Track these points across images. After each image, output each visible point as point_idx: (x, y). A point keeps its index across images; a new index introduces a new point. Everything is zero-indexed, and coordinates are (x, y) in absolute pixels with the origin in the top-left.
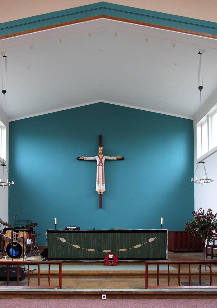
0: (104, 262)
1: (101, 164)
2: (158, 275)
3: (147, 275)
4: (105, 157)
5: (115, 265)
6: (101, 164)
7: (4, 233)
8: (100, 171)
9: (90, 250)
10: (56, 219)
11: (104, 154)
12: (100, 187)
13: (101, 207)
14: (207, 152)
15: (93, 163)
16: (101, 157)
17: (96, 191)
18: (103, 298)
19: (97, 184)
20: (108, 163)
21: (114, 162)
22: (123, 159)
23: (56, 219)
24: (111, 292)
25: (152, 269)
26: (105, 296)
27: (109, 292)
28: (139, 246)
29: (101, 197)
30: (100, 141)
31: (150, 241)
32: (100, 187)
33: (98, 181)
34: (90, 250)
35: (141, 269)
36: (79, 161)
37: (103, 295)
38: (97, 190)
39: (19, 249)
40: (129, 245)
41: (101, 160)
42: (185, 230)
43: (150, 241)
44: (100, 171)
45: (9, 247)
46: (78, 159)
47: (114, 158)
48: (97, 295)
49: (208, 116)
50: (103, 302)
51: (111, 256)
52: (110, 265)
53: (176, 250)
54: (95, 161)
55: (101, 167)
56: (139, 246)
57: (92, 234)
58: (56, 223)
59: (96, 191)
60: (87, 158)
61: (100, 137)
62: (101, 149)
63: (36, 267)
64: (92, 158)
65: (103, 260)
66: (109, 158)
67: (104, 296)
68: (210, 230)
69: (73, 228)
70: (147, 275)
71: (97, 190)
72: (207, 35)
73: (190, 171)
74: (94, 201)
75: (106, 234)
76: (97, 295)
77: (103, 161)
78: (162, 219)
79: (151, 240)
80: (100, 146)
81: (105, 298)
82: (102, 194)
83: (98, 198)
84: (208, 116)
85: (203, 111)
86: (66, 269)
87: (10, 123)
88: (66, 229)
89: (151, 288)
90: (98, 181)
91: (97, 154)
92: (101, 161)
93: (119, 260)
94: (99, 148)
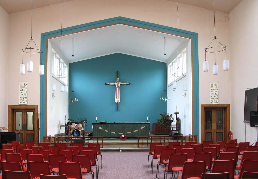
0: (120, 139)
1: (118, 87)
2: (143, 144)
3: (138, 144)
4: (120, 83)
5: (125, 140)
6: (118, 87)
7: (71, 125)
8: (117, 90)
9: (113, 133)
10: (97, 118)
11: (120, 81)
12: (118, 100)
13: (118, 110)
14: (172, 81)
15: (114, 86)
16: (118, 83)
17: (115, 101)
18: (120, 152)
19: (116, 98)
20: (121, 86)
21: (124, 86)
22: (129, 84)
23: (97, 118)
24: (123, 149)
25: (141, 141)
26: (121, 151)
27: (122, 149)
28: (137, 131)
29: (118, 105)
30: (118, 75)
31: (142, 128)
32: (118, 100)
33: (116, 96)
34: (113, 133)
35: (136, 141)
36: (106, 85)
37: (120, 151)
38: (116, 101)
39: (79, 133)
40: (132, 130)
41: (118, 85)
42: (157, 123)
43: (142, 128)
44: (117, 90)
45: (74, 132)
46: (106, 84)
47: (125, 83)
48: (118, 151)
49: (173, 62)
50: (120, 153)
51: (123, 136)
52: (123, 140)
53: (157, 133)
54: (115, 85)
55: (118, 89)
56: (137, 131)
57: (114, 125)
58: (97, 120)
59: (115, 101)
60: (111, 84)
61: (118, 72)
62: (118, 79)
63: (87, 141)
64: (113, 84)
65: (120, 138)
66: (122, 83)
67: (121, 151)
68: (168, 123)
69: (104, 122)
70: (138, 144)
71: (116, 101)
72: (166, 32)
73: (164, 93)
74: (114, 107)
75: (121, 125)
76: (118, 151)
77: (119, 85)
78: (147, 117)
79: (142, 128)
80: (118, 77)
81: (121, 152)
82: (118, 103)
83: (116, 105)
84: (182, 53)
85: (171, 59)
86: (104, 142)
87: (69, 64)
88: (100, 122)
89: (140, 148)
90: (116, 96)
91: (116, 81)
92: (118, 85)
93: (127, 138)
94: (117, 78)
